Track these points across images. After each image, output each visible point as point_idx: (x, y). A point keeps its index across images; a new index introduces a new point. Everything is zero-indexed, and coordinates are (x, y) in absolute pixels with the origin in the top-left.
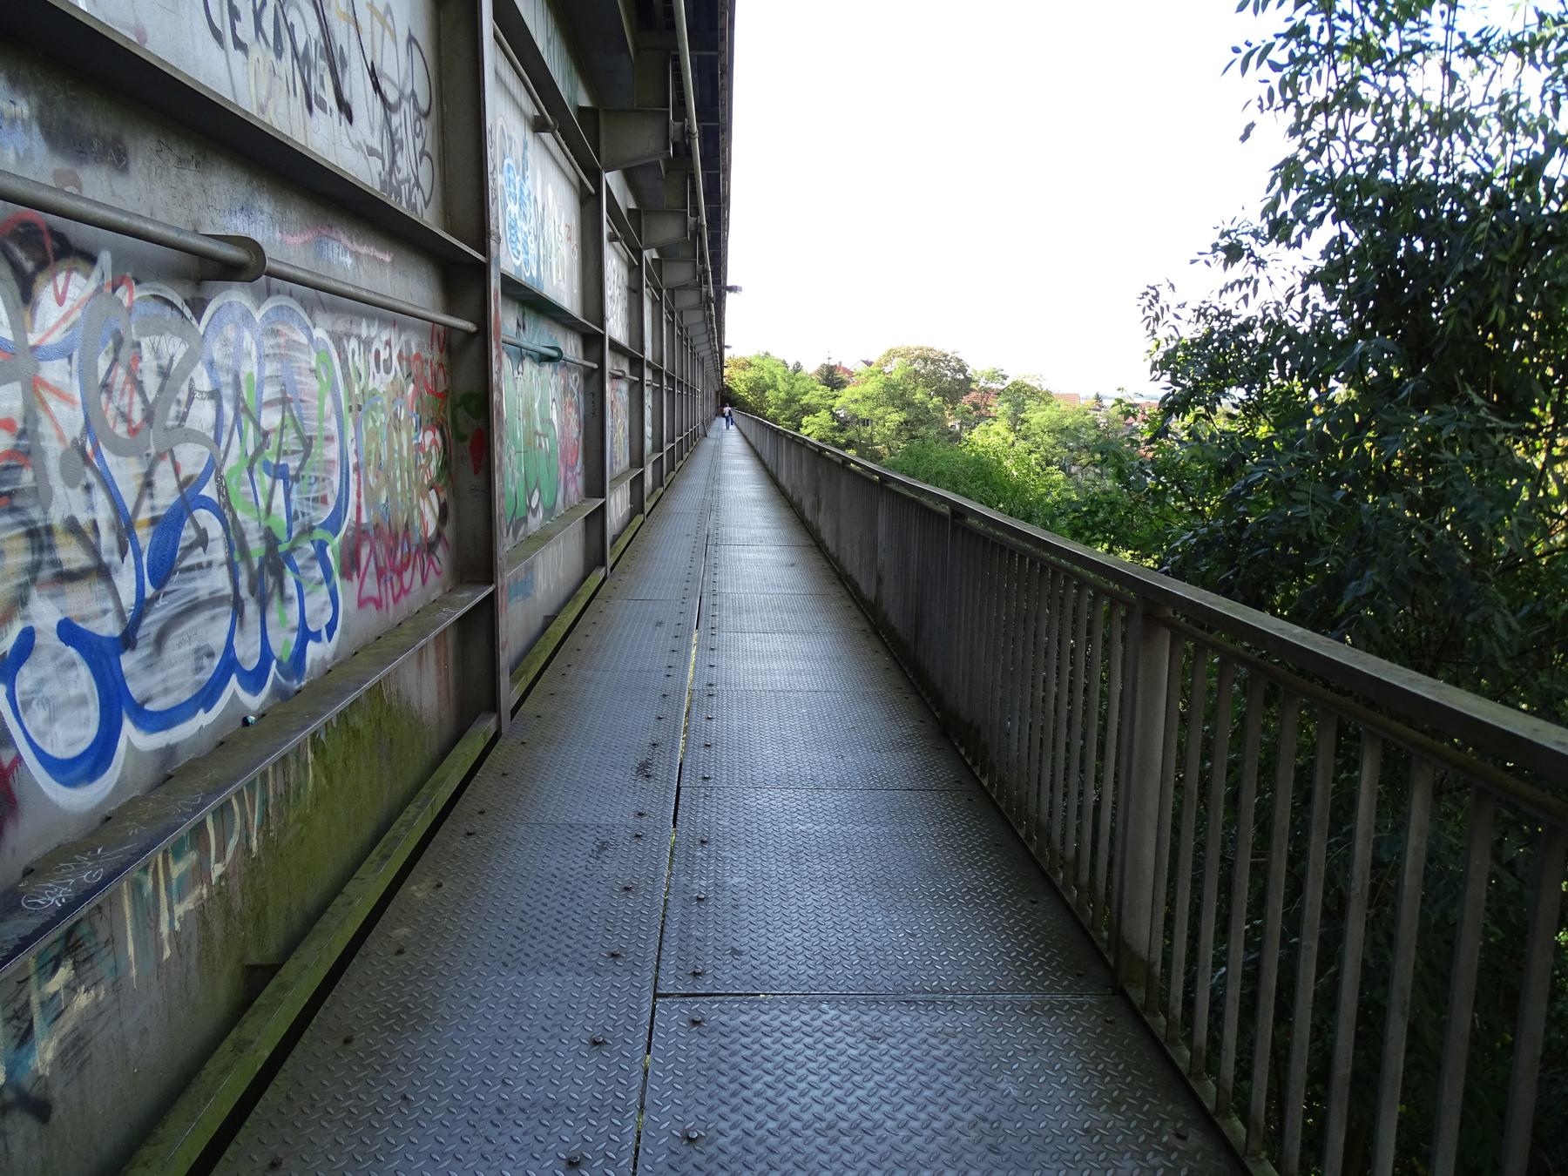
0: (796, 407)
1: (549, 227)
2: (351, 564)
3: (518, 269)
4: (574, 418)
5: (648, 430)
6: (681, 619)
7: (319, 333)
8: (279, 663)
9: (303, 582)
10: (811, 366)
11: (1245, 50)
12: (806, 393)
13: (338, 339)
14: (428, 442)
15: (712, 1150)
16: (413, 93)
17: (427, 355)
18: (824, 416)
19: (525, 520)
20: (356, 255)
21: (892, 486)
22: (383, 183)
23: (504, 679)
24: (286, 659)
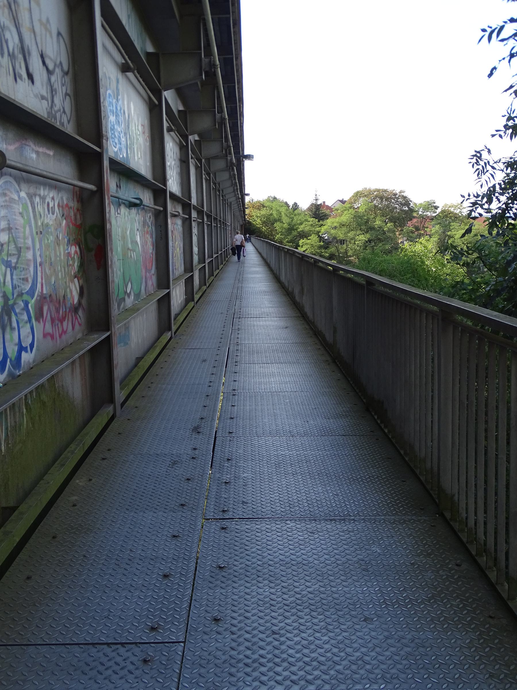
0: (295, 233)
1: (132, 127)
2: (39, 315)
3: (116, 153)
4: (150, 241)
5: (195, 249)
6: (217, 358)
7: (23, 194)
8: (11, 360)
9: (20, 321)
10: (304, 205)
11: (489, 30)
12: (301, 224)
13: (31, 197)
14: (73, 252)
15: (231, 571)
16: (61, 63)
17: (71, 204)
18: (314, 238)
19: (124, 299)
20: (37, 153)
21: (320, 264)
22: (48, 113)
23: (117, 386)
24: (13, 359)
